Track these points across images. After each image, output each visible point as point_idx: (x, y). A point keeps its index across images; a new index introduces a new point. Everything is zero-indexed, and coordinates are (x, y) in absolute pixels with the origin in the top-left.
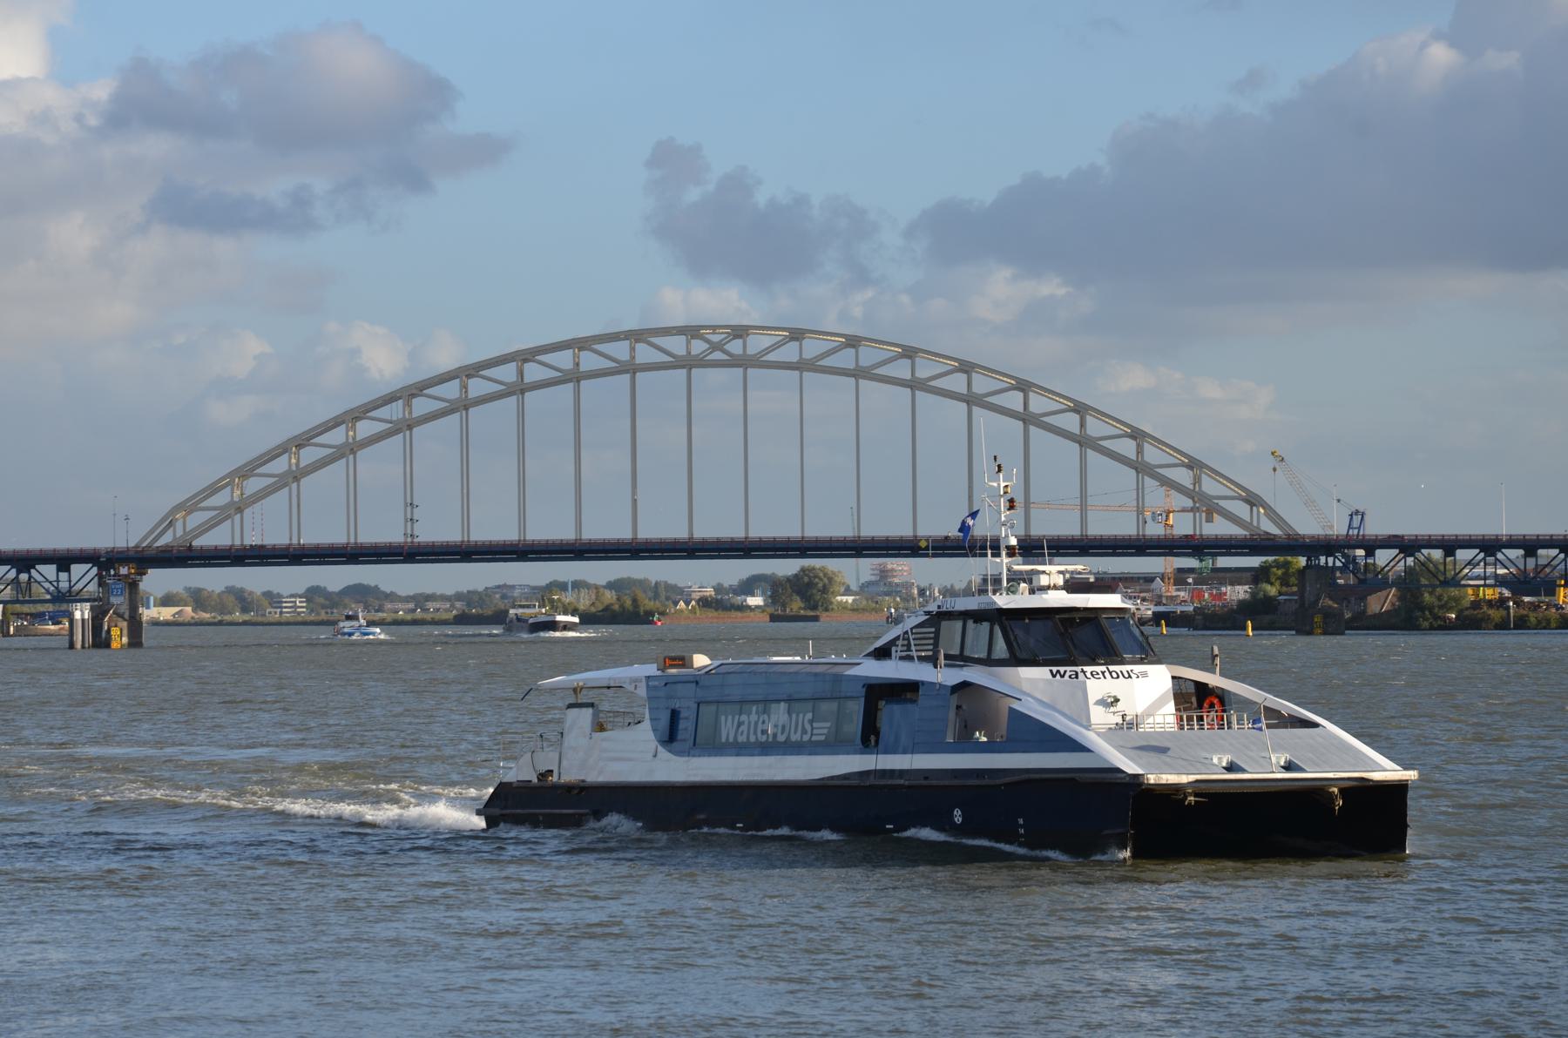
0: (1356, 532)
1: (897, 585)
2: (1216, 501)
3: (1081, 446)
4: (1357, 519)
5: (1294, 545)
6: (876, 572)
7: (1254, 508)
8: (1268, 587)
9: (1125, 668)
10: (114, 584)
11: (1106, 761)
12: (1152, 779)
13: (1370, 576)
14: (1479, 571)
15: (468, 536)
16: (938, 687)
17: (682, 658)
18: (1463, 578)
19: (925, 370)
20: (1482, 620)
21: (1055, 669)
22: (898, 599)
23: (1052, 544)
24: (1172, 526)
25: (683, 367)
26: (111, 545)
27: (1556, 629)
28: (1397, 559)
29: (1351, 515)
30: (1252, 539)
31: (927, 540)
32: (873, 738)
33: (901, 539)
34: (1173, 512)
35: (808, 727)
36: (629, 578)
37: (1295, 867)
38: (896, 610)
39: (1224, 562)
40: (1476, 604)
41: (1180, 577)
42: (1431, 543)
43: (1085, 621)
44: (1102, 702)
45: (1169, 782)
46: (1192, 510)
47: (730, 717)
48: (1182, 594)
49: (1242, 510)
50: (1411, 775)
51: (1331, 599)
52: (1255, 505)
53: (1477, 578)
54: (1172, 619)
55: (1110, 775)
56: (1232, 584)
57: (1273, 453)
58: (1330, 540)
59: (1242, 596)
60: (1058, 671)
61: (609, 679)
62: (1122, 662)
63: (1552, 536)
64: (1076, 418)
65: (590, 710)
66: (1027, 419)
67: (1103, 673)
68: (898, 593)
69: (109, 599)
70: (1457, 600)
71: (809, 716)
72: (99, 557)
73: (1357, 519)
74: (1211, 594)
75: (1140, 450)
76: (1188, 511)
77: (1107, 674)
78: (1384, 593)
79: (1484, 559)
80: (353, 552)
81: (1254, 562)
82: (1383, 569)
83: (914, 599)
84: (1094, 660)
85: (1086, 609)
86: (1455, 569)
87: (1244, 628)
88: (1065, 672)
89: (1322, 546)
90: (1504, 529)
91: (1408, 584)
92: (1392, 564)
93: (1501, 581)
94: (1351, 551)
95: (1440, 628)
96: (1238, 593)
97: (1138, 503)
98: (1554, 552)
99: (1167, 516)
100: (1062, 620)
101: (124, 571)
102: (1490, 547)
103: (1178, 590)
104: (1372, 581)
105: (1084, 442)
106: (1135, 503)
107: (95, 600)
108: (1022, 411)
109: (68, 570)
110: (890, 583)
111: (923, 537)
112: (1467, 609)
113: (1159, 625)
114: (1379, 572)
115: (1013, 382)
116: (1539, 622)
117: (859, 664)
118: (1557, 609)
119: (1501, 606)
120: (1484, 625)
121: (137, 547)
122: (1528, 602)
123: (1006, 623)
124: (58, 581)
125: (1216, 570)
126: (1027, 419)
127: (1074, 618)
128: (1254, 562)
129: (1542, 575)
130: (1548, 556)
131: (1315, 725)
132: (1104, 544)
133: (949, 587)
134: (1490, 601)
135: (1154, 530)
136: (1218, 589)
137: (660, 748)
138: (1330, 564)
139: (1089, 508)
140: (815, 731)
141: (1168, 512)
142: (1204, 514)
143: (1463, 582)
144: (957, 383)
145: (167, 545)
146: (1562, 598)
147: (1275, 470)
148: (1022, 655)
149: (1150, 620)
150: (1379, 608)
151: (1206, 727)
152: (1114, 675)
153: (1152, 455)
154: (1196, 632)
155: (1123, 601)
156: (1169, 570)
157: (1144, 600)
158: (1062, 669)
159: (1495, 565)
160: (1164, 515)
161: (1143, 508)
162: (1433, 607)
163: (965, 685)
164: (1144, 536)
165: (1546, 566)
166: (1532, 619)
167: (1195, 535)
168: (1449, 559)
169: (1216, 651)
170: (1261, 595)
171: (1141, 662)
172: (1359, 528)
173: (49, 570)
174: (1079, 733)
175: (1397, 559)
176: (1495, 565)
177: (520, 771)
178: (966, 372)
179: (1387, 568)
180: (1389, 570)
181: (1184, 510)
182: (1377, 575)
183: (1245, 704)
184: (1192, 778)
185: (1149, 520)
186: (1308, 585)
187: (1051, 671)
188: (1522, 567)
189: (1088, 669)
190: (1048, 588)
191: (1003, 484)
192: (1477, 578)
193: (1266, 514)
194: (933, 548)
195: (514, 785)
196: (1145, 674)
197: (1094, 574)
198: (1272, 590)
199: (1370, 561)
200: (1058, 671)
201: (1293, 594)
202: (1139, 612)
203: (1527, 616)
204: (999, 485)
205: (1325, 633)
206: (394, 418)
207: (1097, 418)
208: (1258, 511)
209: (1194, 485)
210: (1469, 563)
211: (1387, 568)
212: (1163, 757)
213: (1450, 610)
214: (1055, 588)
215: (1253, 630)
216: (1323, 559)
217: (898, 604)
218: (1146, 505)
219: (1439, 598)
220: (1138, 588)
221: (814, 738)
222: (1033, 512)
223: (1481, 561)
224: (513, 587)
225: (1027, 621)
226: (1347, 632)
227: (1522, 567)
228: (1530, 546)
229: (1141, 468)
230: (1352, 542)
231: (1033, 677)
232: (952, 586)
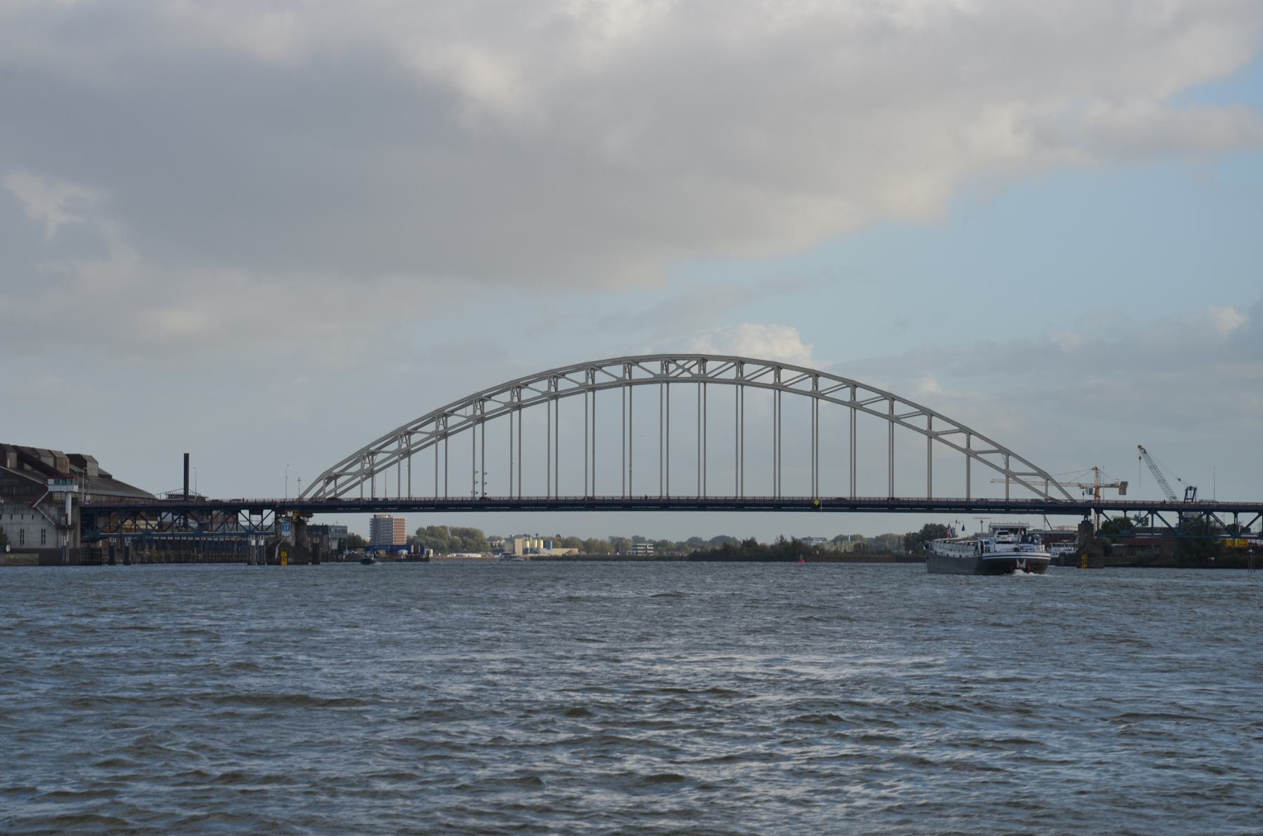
25: (696, 381)
36: (891, 534)
101: (290, 514)
147: (1140, 458)
167: (699, 497)
205: (1089, 567)
206: (468, 415)
224: (812, 539)
226: (1057, 556)
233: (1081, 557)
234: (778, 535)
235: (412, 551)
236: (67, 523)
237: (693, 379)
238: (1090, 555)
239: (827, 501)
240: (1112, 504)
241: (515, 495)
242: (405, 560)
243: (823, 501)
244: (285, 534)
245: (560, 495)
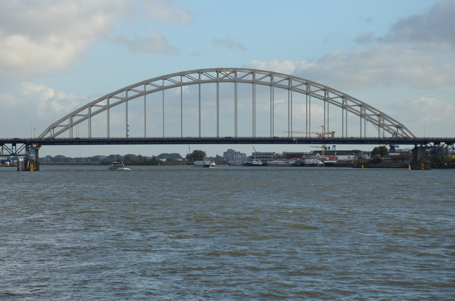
10: (31, 150)
15: (237, 136)
26: (423, 137)
33: (196, 138)
69: (29, 155)
72: (26, 141)
80: (90, 140)
89: (424, 141)
98: (444, 143)
101: (34, 146)
107: (25, 155)
109: (15, 145)
121: (38, 138)
124: (12, 149)
145: (48, 138)
154: (354, 169)
173: (9, 146)
205: (425, 169)
233: (421, 164)
234: (207, 154)
235: (11, 162)
237: (230, 81)
238: (426, 164)
239: (299, 139)
241: (363, 136)
242: (9, 166)
243: (298, 139)
244: (31, 155)
245: (366, 136)
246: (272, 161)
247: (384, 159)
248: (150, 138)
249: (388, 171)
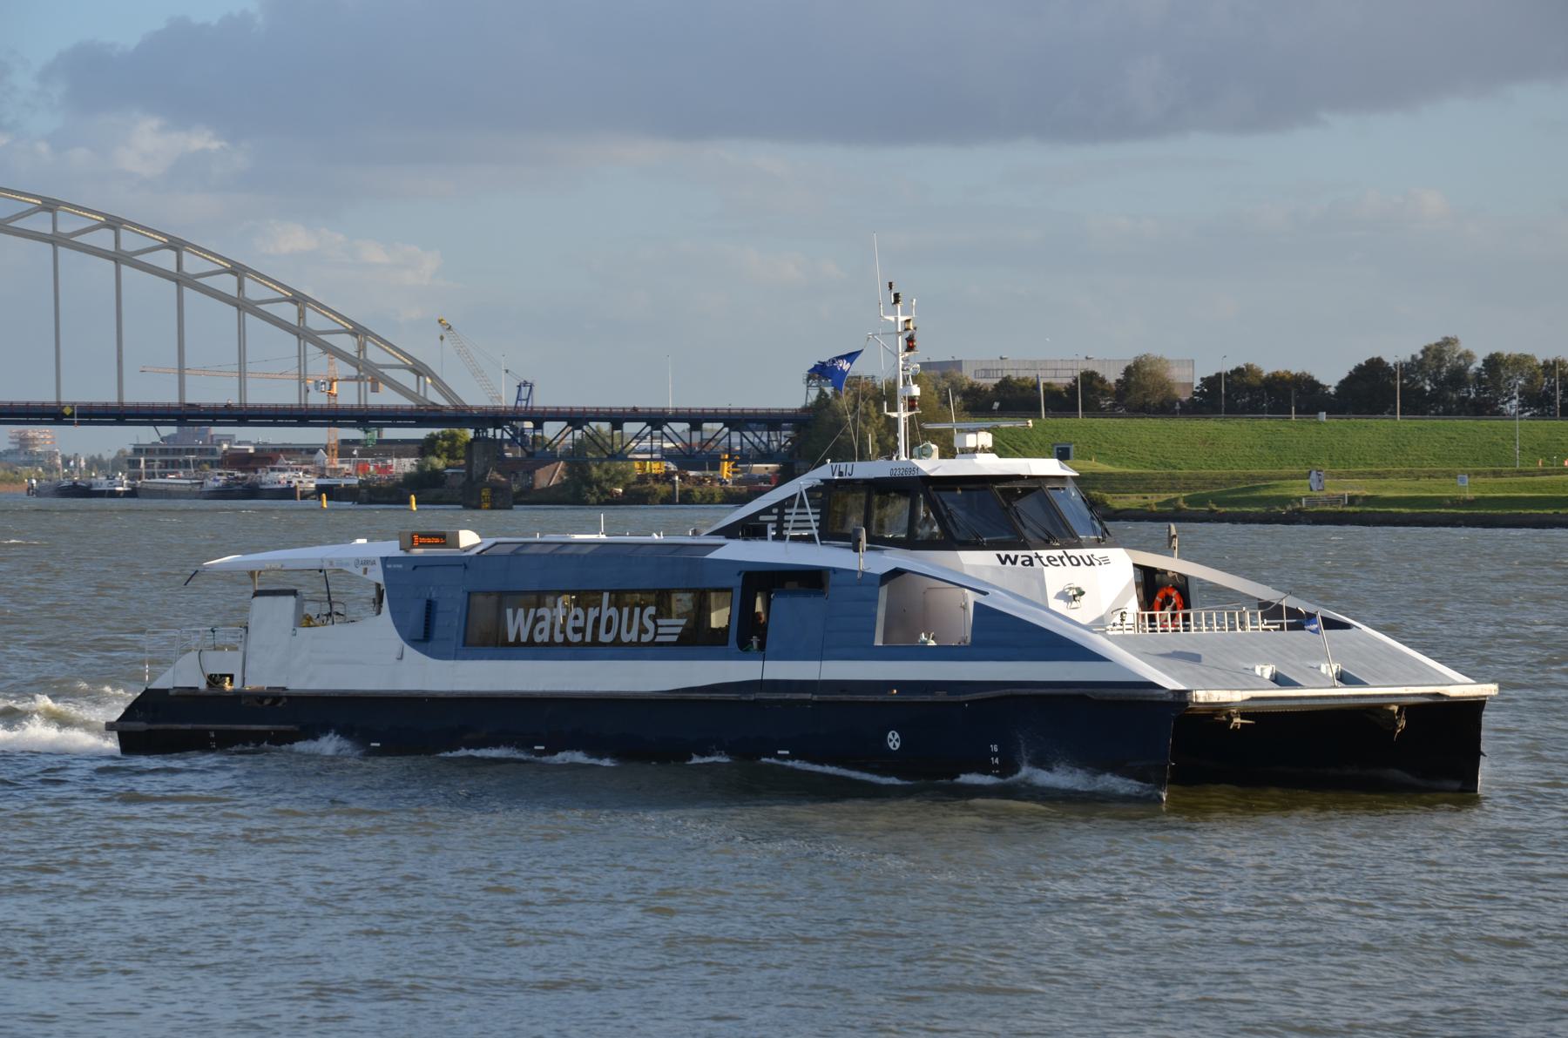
0: (524, 403)
1: (39, 454)
2: (381, 370)
3: (239, 309)
4: (525, 390)
5: (462, 417)
6: (15, 440)
7: (421, 378)
8: (435, 460)
9: (1085, 552)
11: (1139, 676)
12: (1202, 696)
13: (538, 449)
14: (645, 444)
16: (859, 575)
17: (442, 536)
18: (629, 452)
19: (67, 224)
20: (648, 494)
21: (1003, 554)
22: (40, 470)
23: (83, 411)
24: (336, 396)
27: (719, 503)
28: (565, 432)
29: (519, 387)
30: (418, 410)
31: (72, 407)
32: (755, 640)
33: (43, 406)
34: (337, 380)
35: (649, 625)
37: (1372, 808)
38: (38, 481)
39: (390, 433)
40: (643, 479)
41: (344, 449)
42: (599, 416)
43: (1026, 492)
44: (1062, 595)
45: (1221, 700)
46: (356, 379)
47: (521, 612)
48: (346, 466)
49: (407, 379)
50: (1489, 689)
51: (499, 472)
52: (422, 375)
53: (644, 452)
54: (333, 493)
55: (1141, 692)
56: (398, 456)
57: (440, 321)
58: (498, 412)
59: (408, 469)
60: (1007, 557)
61: (322, 560)
62: (1079, 545)
63: (703, 409)
64: (233, 279)
65: (291, 600)
66: (181, 279)
67: (1061, 558)
68: (40, 463)
70: (624, 474)
71: (651, 610)
73: (525, 390)
74: (376, 467)
75: (301, 315)
76: (351, 380)
77: (1065, 560)
78: (552, 466)
79: (651, 432)
81: (421, 433)
82: (551, 442)
83: (58, 470)
84: (1048, 542)
85: (1031, 477)
86: (622, 443)
87: (408, 502)
88: (1016, 557)
89: (490, 418)
90: (670, 403)
91: (576, 458)
92: (560, 437)
93: (667, 455)
94: (519, 423)
95: (608, 503)
96: (404, 465)
97: (300, 371)
98: (719, 426)
99: (331, 386)
100: (1002, 491)
102: (657, 420)
103: (342, 462)
104: (540, 455)
105: (242, 305)
106: (297, 370)
108: (175, 271)
110: (31, 452)
111: (68, 403)
112: (634, 483)
113: (320, 499)
114: (547, 445)
115: (164, 240)
116: (704, 497)
117: (722, 545)
118: (721, 484)
119: (667, 480)
120: (650, 500)
122: (693, 477)
123: (934, 494)
125: (381, 442)
126: (181, 279)
127: (1015, 489)
128: (421, 433)
129: (706, 449)
130: (712, 430)
131: (1347, 626)
132: (264, 413)
133: (96, 456)
134: (656, 475)
135: (317, 399)
136: (383, 462)
137: (408, 650)
138: (498, 437)
139: (248, 375)
140: (661, 630)
141: (332, 381)
142: (369, 384)
143: (630, 456)
144: (104, 239)
146: (726, 472)
147: (442, 338)
148: (960, 536)
149: (313, 493)
150: (547, 481)
151: (1159, 629)
152: (1075, 562)
153: (314, 320)
155: (1062, 468)
156: (333, 442)
157: (306, 472)
158: (1012, 554)
159: (662, 438)
160: (328, 383)
161: (305, 375)
162: (601, 481)
163: (897, 573)
164: (366, 405)
165: (710, 440)
166: (697, 494)
168: (616, 432)
169: (1174, 532)
170: (428, 468)
171: (1098, 544)
172: (527, 400)
174: (1086, 638)
175: (565, 432)
176: (662, 438)
177: (184, 675)
178: (113, 228)
179: (555, 442)
180: (558, 443)
181: (348, 379)
182: (545, 448)
183: (1220, 595)
184: (1247, 695)
185: (312, 388)
186: (475, 458)
187: (999, 556)
188: (688, 441)
189: (1044, 553)
190: (975, 450)
191: (902, 319)
192: (644, 452)
193: (433, 384)
194: (79, 416)
195: (171, 693)
196: (1106, 561)
197: (254, 445)
198: (439, 463)
199: (538, 433)
200: (1007, 557)
201: (461, 467)
202: (302, 485)
203: (692, 491)
204: (896, 319)
205: (493, 508)
207: (256, 280)
208: (425, 382)
209: (359, 352)
210: (636, 437)
211: (555, 442)
212: (1196, 666)
213: (617, 484)
214: (984, 450)
215: (417, 503)
216: (491, 431)
217: (39, 474)
218: (309, 373)
219: (607, 472)
220: (300, 459)
221: (659, 639)
222: (188, 379)
223: (647, 435)
225: (959, 492)
227: (688, 441)
228: (696, 420)
229: (303, 334)
230: (521, 414)
231: (977, 562)
232: (100, 456)
233: (480, 493)
236: (463, 474)
240: (552, 413)
243: (79, 407)
246: (154, 478)
247: (453, 473)
248: (756, 414)
249: (534, 512)
